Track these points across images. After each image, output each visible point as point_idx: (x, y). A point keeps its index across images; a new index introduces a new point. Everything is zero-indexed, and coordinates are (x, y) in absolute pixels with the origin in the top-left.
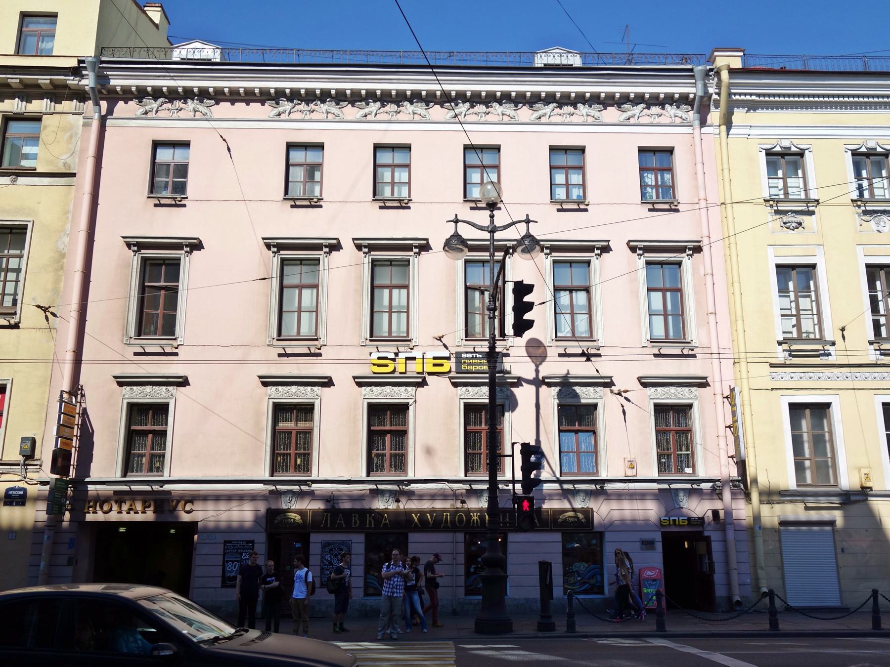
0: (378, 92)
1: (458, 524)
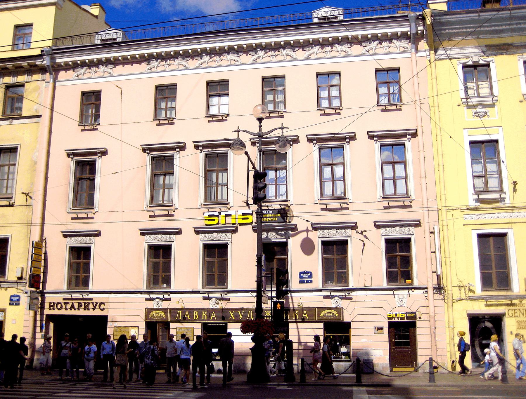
0: (263, 44)
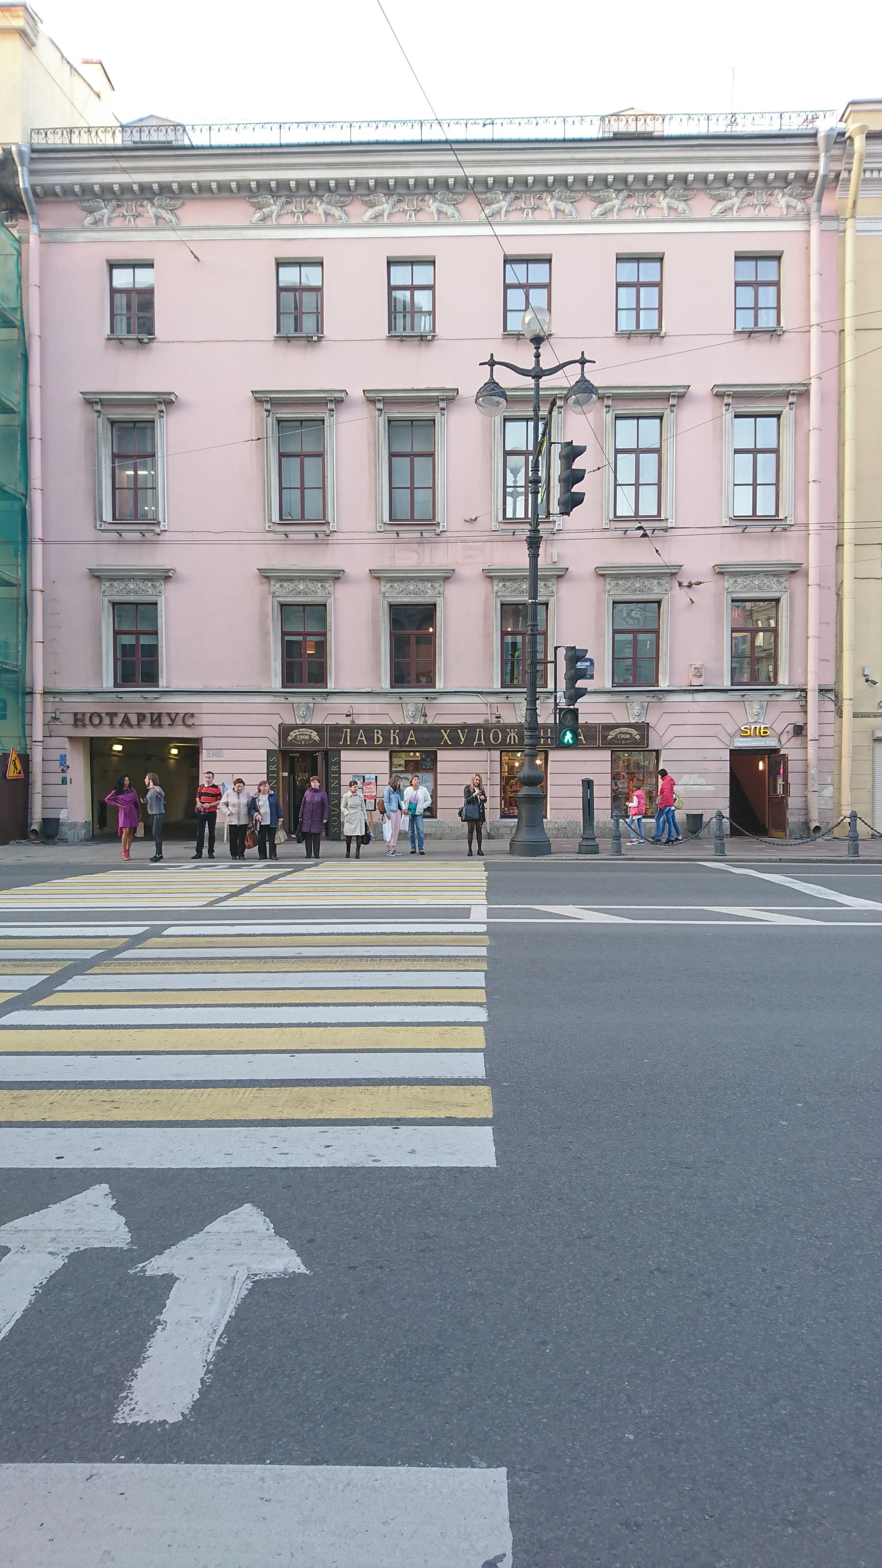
1: (492, 741)
